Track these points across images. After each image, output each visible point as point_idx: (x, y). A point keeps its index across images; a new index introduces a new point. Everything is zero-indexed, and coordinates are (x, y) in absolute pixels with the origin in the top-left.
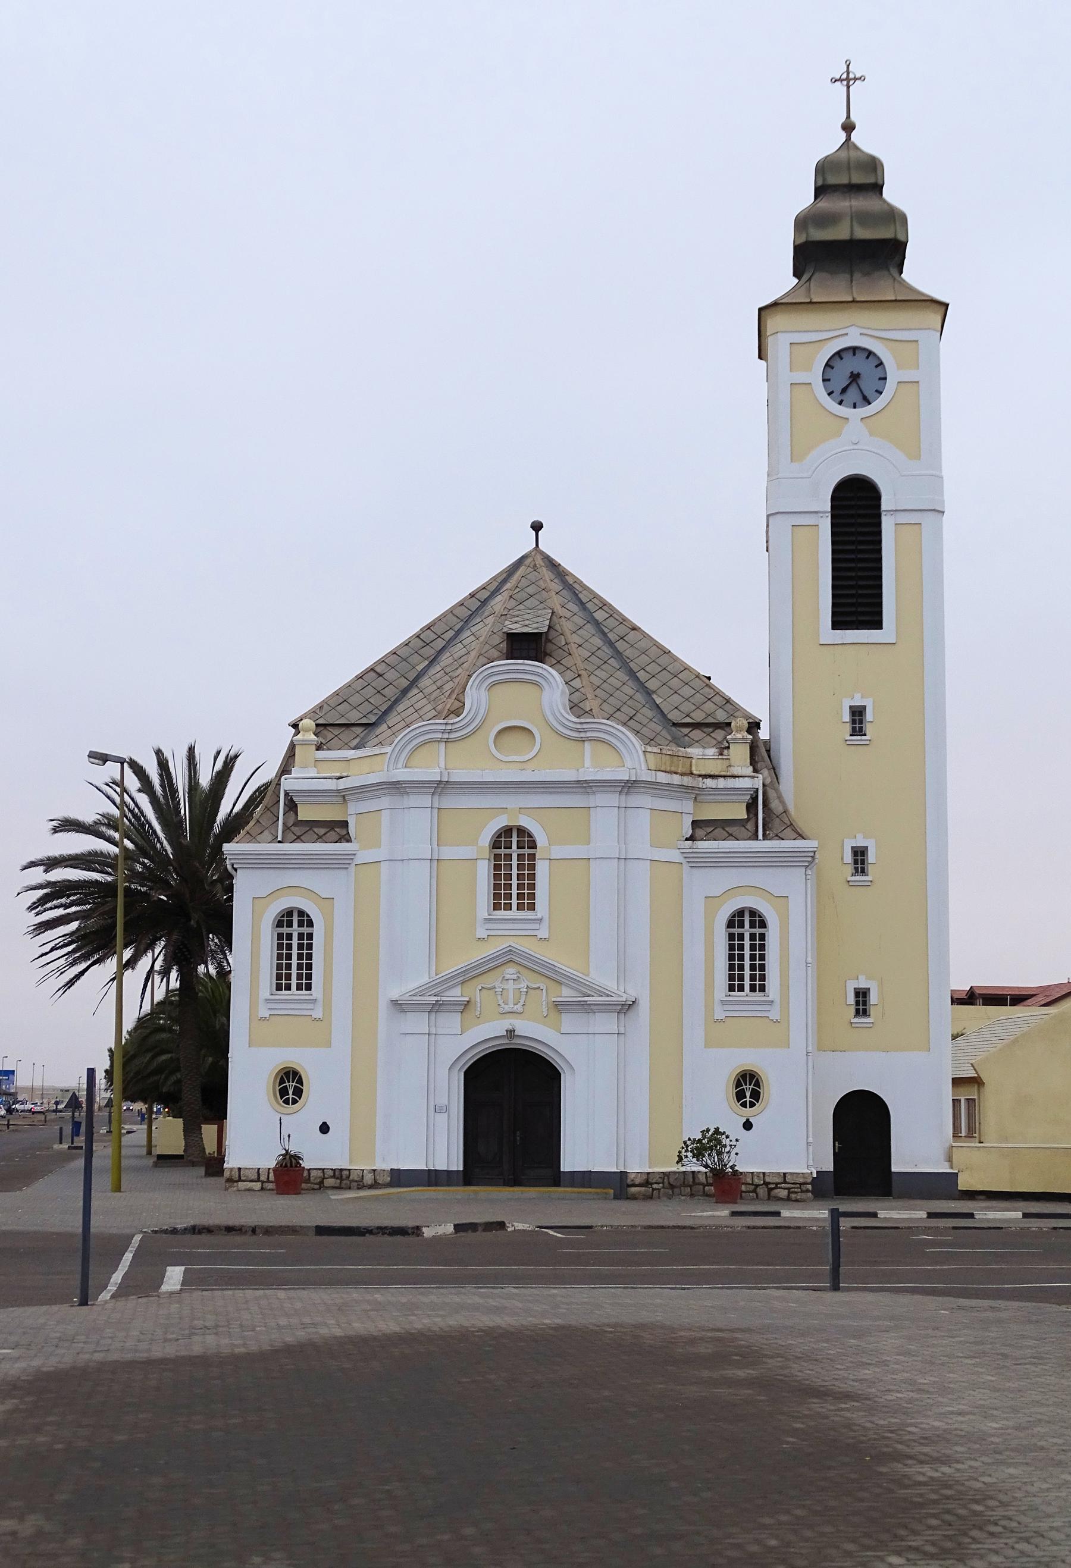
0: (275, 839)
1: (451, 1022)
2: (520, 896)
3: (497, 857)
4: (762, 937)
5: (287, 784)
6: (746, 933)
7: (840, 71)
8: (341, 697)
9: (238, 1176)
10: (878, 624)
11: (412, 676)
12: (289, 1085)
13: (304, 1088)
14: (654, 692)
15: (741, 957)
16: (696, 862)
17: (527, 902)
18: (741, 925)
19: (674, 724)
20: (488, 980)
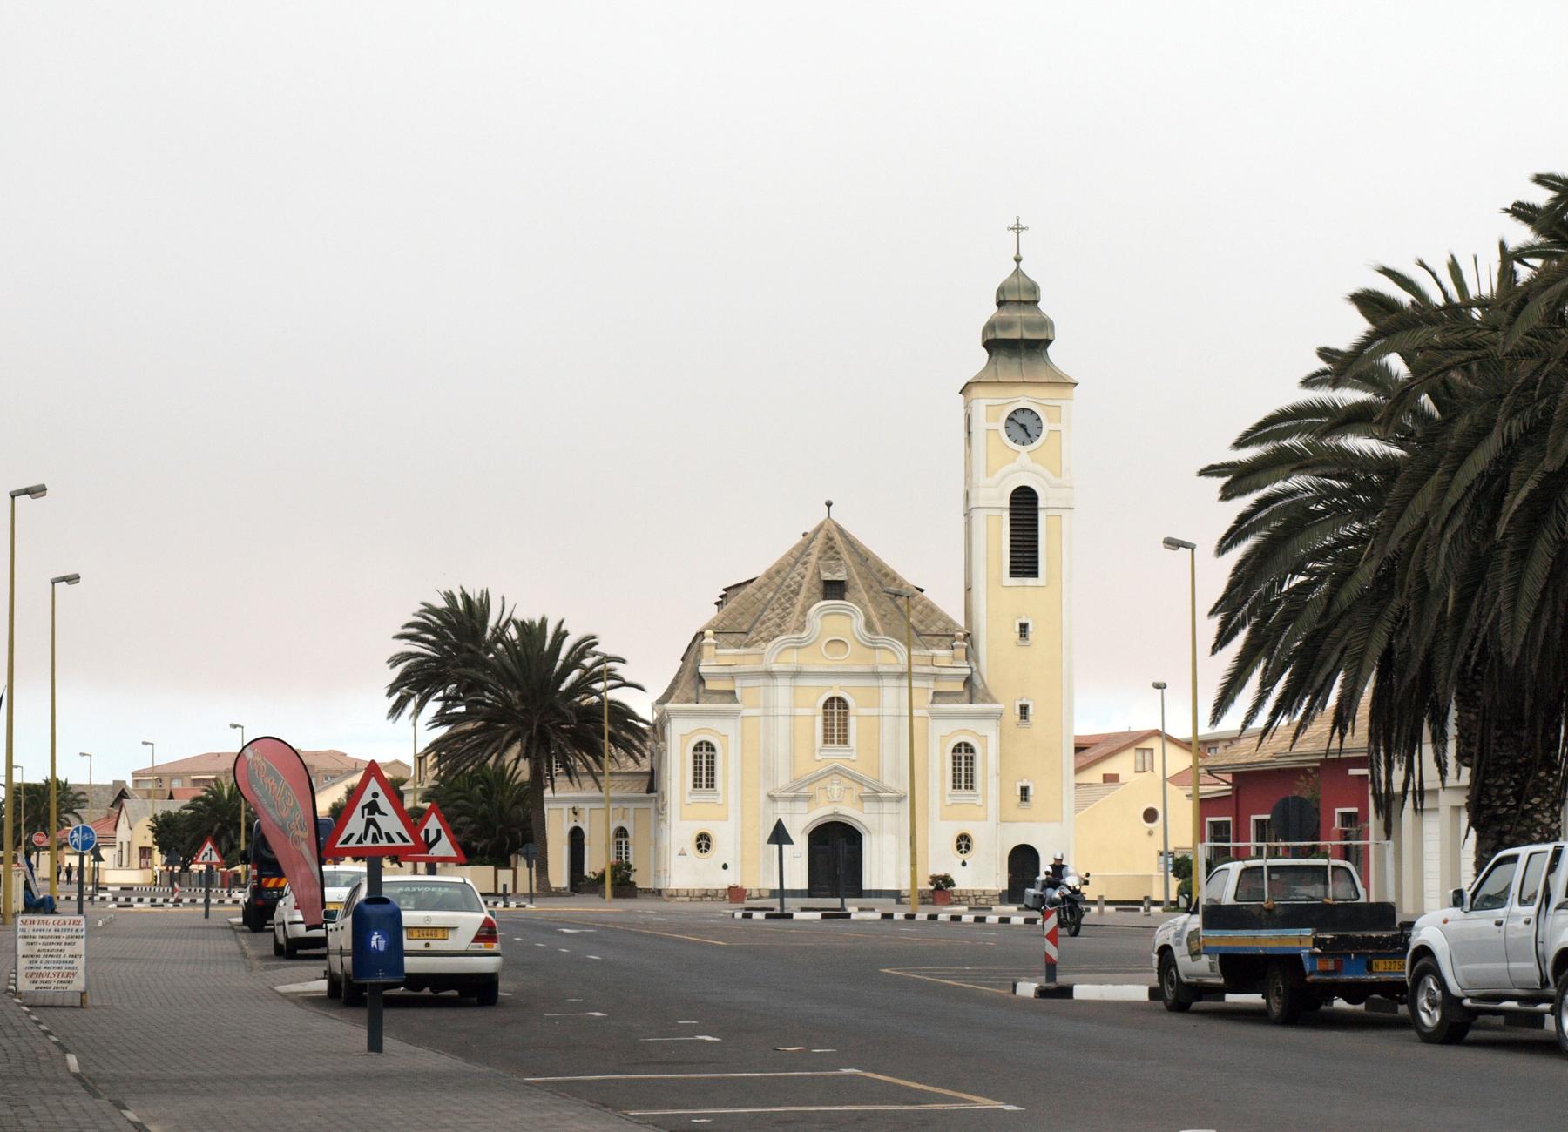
6: (963, 754)
7: (1013, 223)
12: (703, 842)
17: (844, 740)
20: (823, 783)
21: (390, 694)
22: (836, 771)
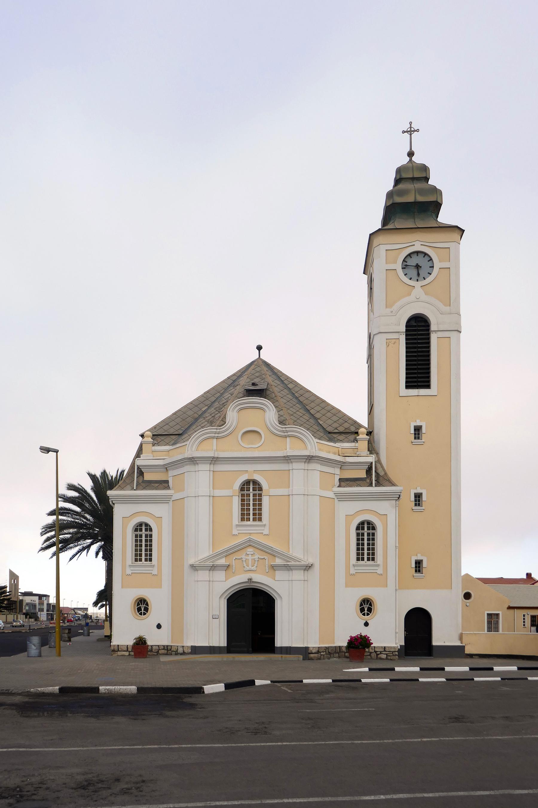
0: (132, 489)
1: (220, 575)
2: (254, 514)
3: (243, 495)
4: (373, 534)
5: (138, 462)
6: (366, 533)
7: (406, 127)
8: (165, 422)
9: (118, 649)
10: (428, 386)
11: (200, 413)
12: (142, 606)
13: (149, 607)
14: (319, 419)
15: (363, 544)
16: (342, 498)
17: (258, 517)
18: (363, 529)
19: (329, 433)
21: (42, 534)
22: (250, 544)
